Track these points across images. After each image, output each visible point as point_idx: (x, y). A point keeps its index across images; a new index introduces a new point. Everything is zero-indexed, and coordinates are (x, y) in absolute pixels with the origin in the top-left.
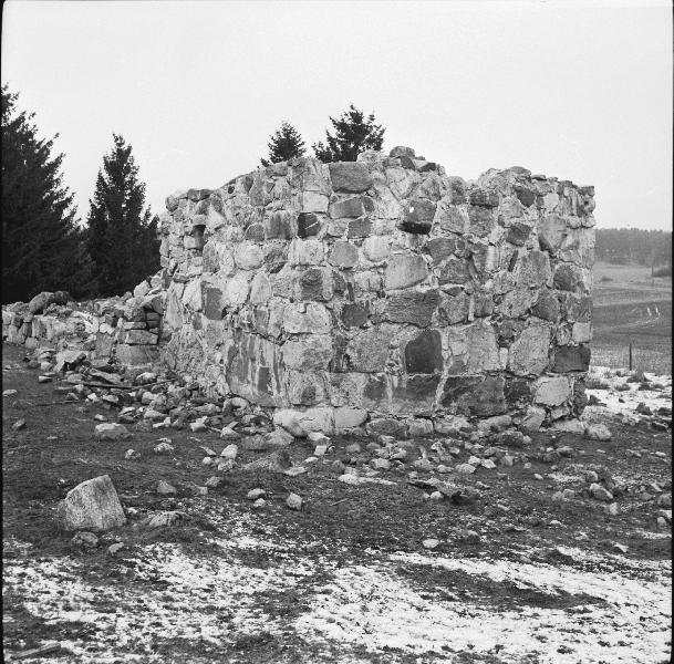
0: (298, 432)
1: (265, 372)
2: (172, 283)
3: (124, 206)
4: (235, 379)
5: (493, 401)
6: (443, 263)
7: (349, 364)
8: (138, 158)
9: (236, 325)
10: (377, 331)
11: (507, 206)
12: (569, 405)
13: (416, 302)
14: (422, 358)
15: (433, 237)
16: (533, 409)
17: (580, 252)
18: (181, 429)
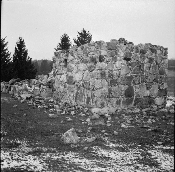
0: (100, 114)
1: (88, 99)
2: (57, 75)
3: (22, 55)
4: (78, 101)
5: (146, 104)
6: (134, 68)
7: (112, 95)
8: (26, 43)
9: (78, 86)
10: (119, 86)
11: (148, 52)
12: (163, 105)
13: (128, 79)
14: (129, 93)
15: (131, 62)
16: (155, 106)
17: (165, 65)
18: (69, 114)
